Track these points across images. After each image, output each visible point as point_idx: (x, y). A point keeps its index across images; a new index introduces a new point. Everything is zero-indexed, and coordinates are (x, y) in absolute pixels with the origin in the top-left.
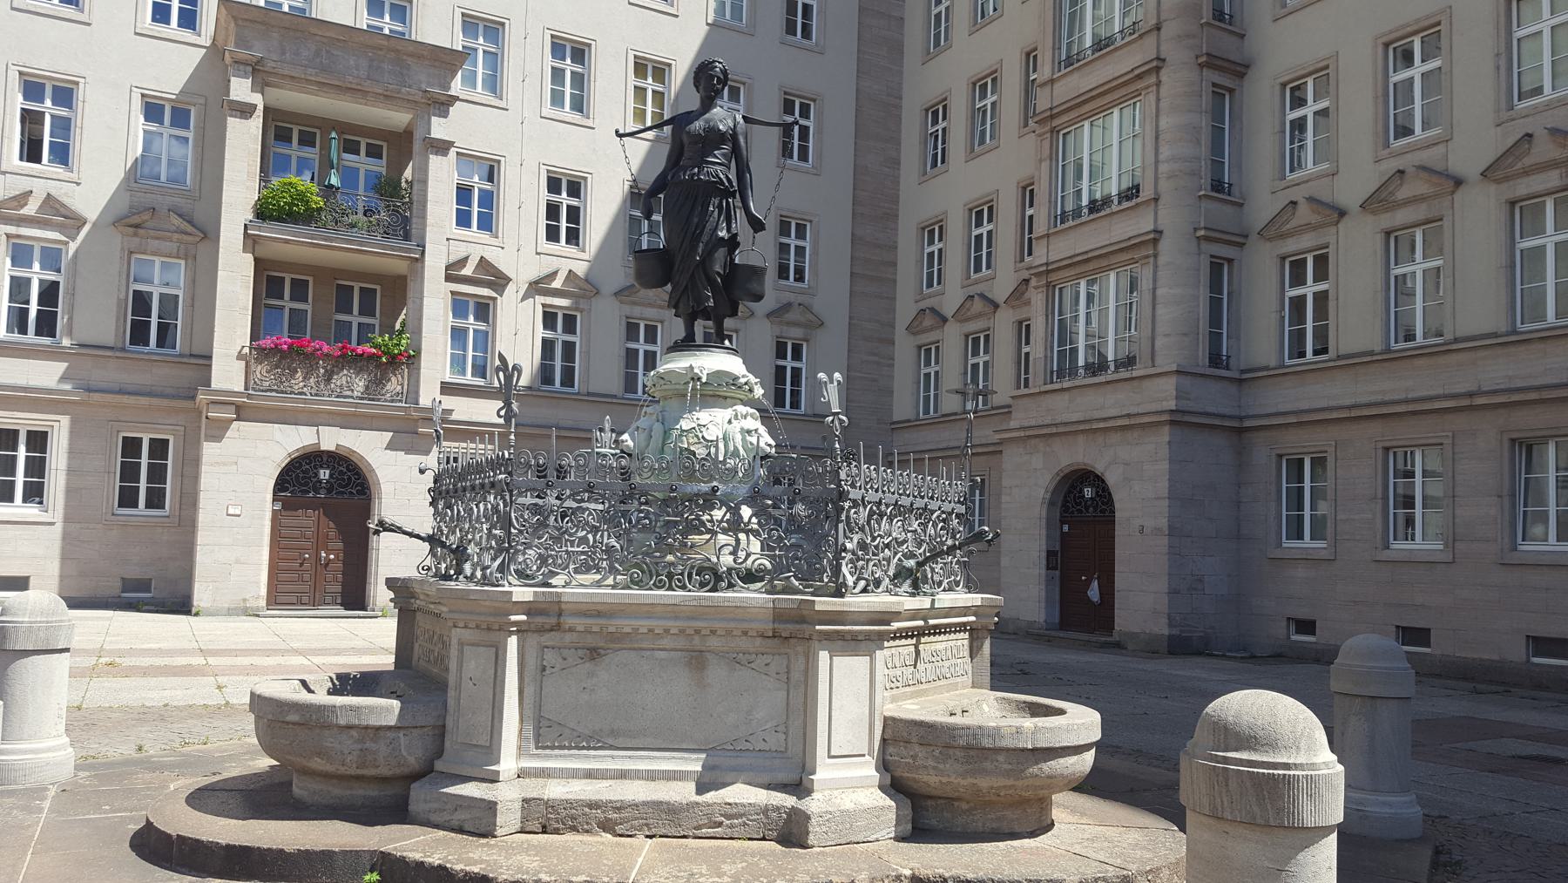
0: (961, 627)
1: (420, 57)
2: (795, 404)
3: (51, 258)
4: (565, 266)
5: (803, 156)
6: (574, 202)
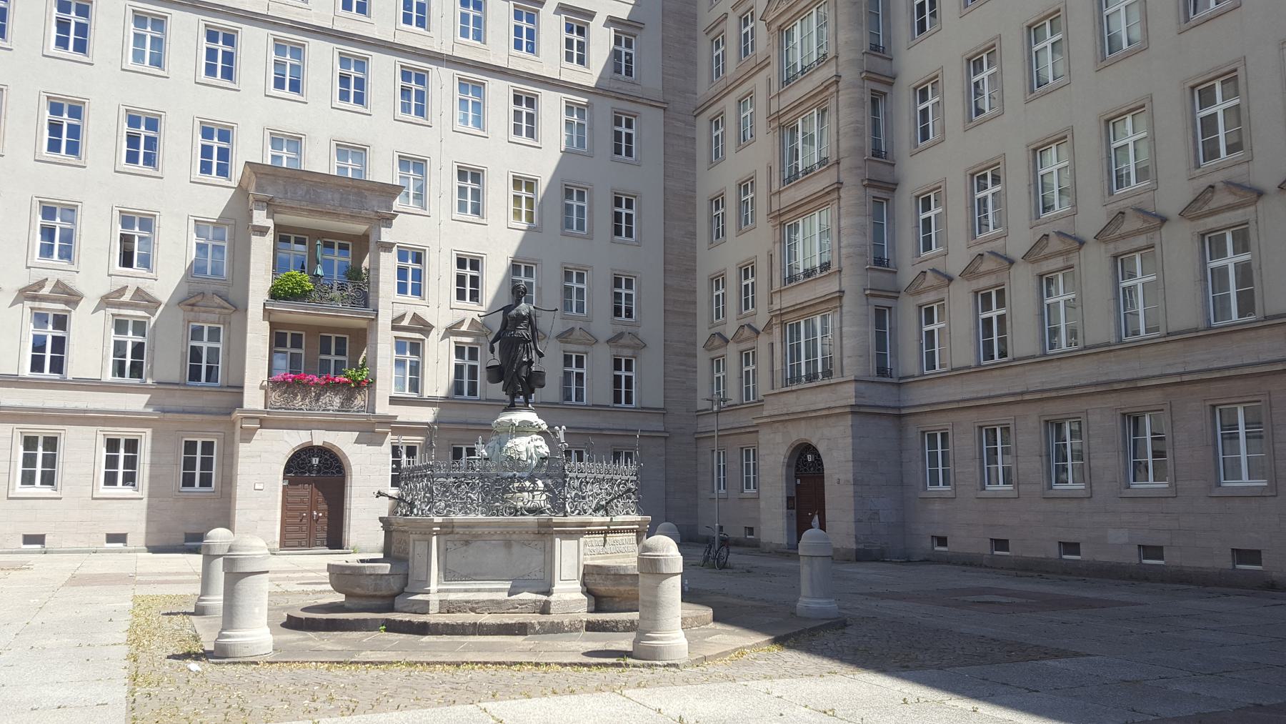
0: (632, 531)
1: (373, 190)
2: (629, 400)
3: (139, 327)
4: (470, 316)
5: (629, 234)
6: (475, 273)
